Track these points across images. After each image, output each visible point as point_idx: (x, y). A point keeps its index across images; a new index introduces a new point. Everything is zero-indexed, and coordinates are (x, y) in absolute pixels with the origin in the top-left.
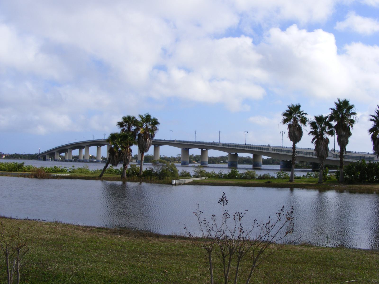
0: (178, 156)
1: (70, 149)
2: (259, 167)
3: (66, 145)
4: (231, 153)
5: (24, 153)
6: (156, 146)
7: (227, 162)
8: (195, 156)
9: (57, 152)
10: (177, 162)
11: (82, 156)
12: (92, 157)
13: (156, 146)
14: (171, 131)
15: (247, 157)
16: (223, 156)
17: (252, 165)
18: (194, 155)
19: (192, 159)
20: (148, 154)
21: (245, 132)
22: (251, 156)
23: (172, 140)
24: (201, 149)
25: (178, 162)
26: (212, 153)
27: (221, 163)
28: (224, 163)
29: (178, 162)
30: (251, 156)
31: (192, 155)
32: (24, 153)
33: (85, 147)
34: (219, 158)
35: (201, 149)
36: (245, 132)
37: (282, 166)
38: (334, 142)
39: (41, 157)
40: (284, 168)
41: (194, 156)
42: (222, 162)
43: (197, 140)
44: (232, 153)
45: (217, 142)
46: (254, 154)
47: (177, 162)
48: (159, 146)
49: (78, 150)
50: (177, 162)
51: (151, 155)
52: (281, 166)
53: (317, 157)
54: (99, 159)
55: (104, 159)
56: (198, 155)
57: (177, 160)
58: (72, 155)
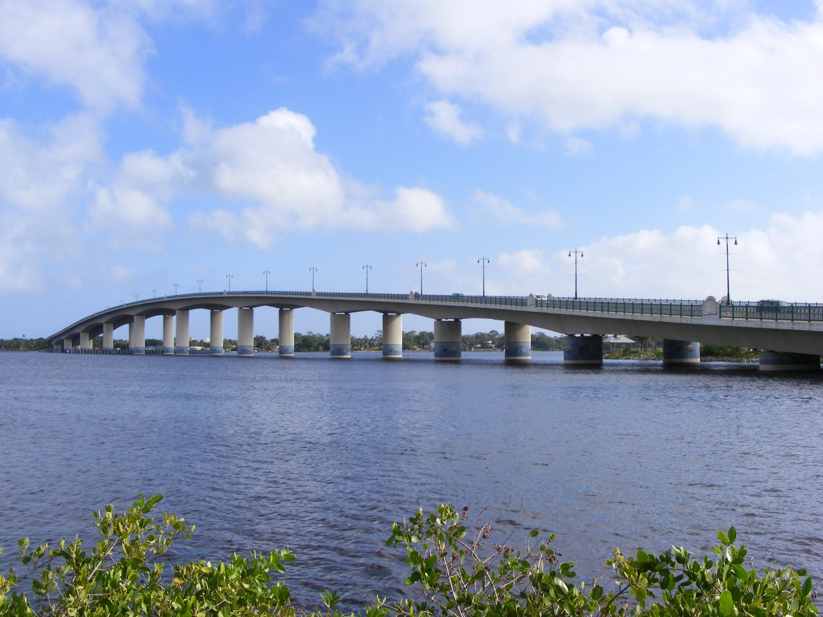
0: (377, 335)
1: (106, 323)
2: (679, 361)
3: (97, 313)
4: (443, 320)
5: (24, 336)
6: (389, 314)
7: (490, 345)
8: (417, 334)
9: (84, 331)
10: (375, 350)
11: (223, 339)
12: (149, 343)
13: (389, 314)
14: (266, 272)
15: (538, 334)
16: (483, 332)
17: (503, 353)
18: (416, 332)
19: (410, 340)
20: (311, 333)
21: (481, 261)
22: (498, 326)
23: (491, 298)
24: (382, 314)
25: (378, 348)
26: (470, 327)
27: (476, 348)
28: (484, 349)
29: (378, 348)
30: (498, 326)
31: (410, 332)
32: (24, 336)
33: (135, 317)
34: (472, 337)
35: (382, 314)
36: (481, 261)
37: (568, 352)
38: (728, 270)
39: (56, 344)
40: (574, 358)
41: (416, 334)
42: (479, 345)
43: (587, 292)
44: (445, 320)
45: (566, 296)
46: (508, 321)
47: (377, 350)
48: (291, 309)
49: (128, 324)
50: (377, 350)
51: (318, 334)
52: (565, 352)
53: (175, 317)
54: (168, 346)
55: (206, 347)
56: (425, 332)
57: (375, 345)
58: (190, 336)
